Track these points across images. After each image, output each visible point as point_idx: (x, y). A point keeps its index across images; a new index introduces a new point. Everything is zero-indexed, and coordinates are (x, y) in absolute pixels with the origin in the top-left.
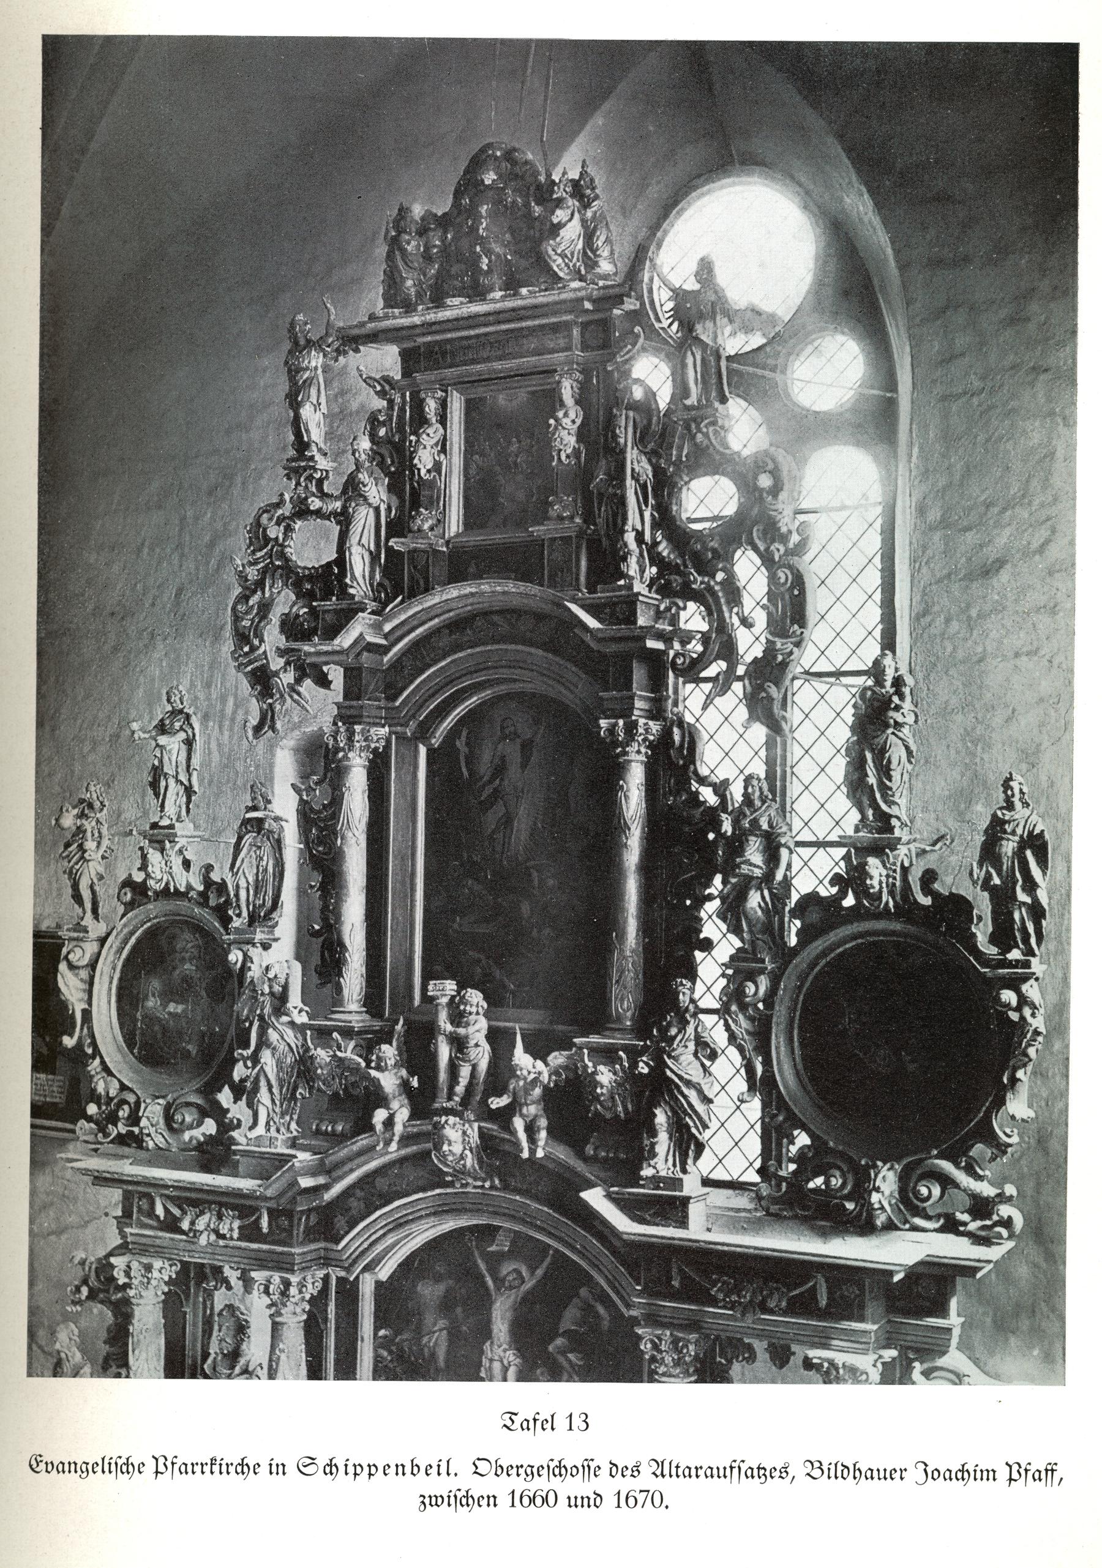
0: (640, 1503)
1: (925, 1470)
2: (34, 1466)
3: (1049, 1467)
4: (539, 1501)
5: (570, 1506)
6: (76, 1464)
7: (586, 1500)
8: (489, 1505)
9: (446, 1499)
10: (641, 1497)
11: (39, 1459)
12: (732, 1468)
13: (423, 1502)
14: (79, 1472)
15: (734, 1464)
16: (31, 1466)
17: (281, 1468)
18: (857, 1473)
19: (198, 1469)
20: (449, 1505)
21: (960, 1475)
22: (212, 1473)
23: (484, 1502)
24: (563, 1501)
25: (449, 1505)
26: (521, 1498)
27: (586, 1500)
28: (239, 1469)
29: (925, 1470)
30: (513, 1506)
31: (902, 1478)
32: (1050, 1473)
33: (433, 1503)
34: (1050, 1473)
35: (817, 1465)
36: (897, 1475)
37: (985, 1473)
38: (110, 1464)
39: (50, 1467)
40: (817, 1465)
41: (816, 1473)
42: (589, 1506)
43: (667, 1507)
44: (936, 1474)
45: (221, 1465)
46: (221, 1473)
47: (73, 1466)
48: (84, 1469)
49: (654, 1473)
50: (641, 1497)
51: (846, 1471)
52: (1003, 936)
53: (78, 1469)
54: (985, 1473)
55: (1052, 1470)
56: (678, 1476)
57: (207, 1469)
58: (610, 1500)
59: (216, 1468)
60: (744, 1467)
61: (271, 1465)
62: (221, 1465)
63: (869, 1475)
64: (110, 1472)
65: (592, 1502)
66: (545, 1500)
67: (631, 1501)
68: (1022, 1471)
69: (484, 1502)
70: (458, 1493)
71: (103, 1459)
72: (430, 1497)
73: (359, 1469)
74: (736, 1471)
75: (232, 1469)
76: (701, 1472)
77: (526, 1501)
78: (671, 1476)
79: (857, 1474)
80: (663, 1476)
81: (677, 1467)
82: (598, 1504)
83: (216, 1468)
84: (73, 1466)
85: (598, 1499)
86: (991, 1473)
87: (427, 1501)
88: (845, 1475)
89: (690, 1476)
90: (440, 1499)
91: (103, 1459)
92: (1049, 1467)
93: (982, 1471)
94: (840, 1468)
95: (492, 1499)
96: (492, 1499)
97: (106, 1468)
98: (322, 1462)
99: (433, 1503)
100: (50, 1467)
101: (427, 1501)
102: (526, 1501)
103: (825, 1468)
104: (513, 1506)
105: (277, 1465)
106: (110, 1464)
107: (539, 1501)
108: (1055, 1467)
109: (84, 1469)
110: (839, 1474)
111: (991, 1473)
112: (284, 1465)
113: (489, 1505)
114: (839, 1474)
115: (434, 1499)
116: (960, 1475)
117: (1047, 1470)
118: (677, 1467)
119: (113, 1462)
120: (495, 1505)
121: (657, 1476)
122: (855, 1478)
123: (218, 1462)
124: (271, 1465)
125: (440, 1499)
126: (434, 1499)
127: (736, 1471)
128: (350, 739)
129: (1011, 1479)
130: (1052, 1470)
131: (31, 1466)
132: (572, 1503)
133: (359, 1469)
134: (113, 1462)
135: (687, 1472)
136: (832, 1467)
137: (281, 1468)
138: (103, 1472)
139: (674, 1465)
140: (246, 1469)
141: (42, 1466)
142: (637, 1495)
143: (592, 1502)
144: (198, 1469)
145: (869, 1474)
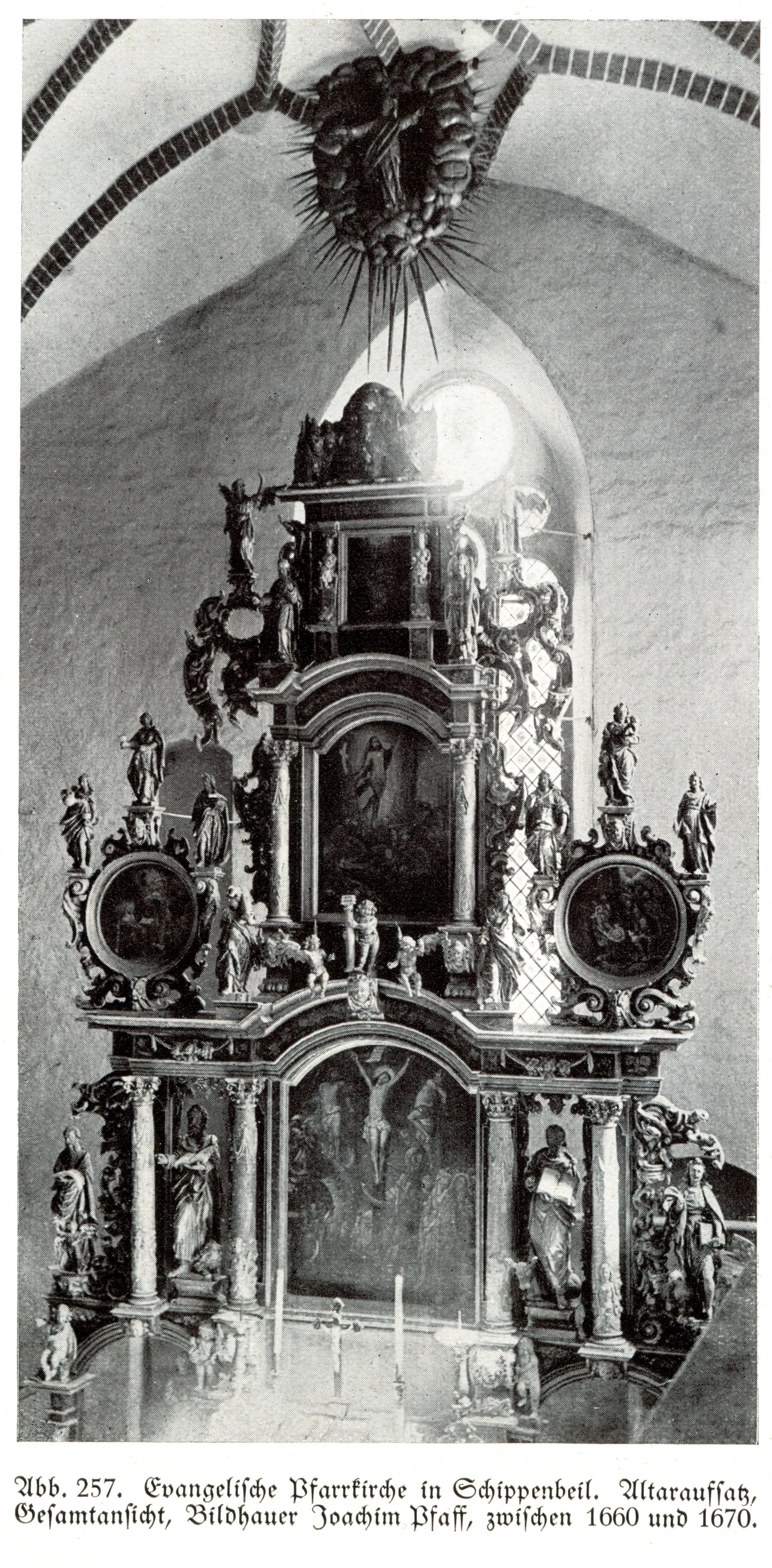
0: (726, 1522)
1: (323, 1515)
2: (151, 1489)
3: (458, 1510)
4: (619, 1519)
5: (652, 1524)
6: (198, 1486)
7: (669, 1519)
8: (562, 1523)
9: (515, 1518)
10: (727, 1517)
11: (156, 1482)
12: (710, 1489)
13: (491, 1521)
14: (202, 1496)
15: (712, 1486)
16: (146, 1489)
17: (435, 1491)
18: (244, 1518)
19: (339, 1492)
20: (518, 1523)
21: (361, 1518)
22: (355, 1496)
23: (557, 1521)
24: (644, 1519)
25: (518, 1523)
26: (602, 1516)
27: (669, 1519)
28: (384, 1492)
29: (323, 1515)
30: (592, 1524)
31: (292, 1523)
32: (459, 1516)
33: (502, 1521)
34: (459, 1516)
35: (199, 1509)
36: (287, 1519)
37: (388, 1517)
38: (237, 1487)
39: (168, 1491)
40: (199, 1509)
41: (199, 1518)
42: (672, 1525)
43: (755, 1525)
44: (335, 1518)
45: (364, 1487)
46: (365, 1496)
47: (195, 1489)
48: (208, 1492)
49: (626, 1495)
50: (727, 1517)
51: (231, 1514)
52: (689, 863)
53: (201, 1492)
54: (388, 1517)
55: (462, 1513)
56: (651, 1498)
57: (349, 1492)
58: (695, 1519)
59: (359, 1491)
60: (724, 1488)
61: (424, 1488)
62: (364, 1487)
63: (256, 1519)
64: (237, 1495)
65: (675, 1521)
66: (626, 1519)
67: (717, 1520)
68: (428, 1514)
69: (557, 1521)
70: (528, 1511)
71: (229, 1482)
72: (499, 1515)
73: (511, 1492)
74: (715, 1493)
75: (376, 1492)
76: (677, 1495)
77: (606, 1519)
78: (643, 1498)
79: (244, 1518)
80: (635, 1497)
81: (651, 1488)
82: (682, 1522)
83: (359, 1491)
84: (195, 1489)
85: (682, 1517)
86: (394, 1517)
87: (495, 1519)
88: (231, 1519)
89: (688, 1498)
90: (509, 1518)
91: (229, 1482)
92: (458, 1510)
93: (384, 1514)
94: (224, 1512)
95: (566, 1517)
96: (566, 1517)
97: (233, 1491)
98: (478, 1484)
99: (502, 1521)
100: (168, 1491)
101: (495, 1519)
102: (606, 1519)
103: (207, 1512)
104: (592, 1524)
105: (431, 1488)
106: (237, 1487)
107: (619, 1519)
108: (464, 1510)
109: (208, 1492)
110: (224, 1518)
111: (394, 1517)
112: (438, 1488)
113: (562, 1523)
114: (224, 1518)
115: (502, 1517)
116: (361, 1518)
117: (455, 1513)
118: (651, 1488)
119: (240, 1485)
120: (569, 1523)
121: (628, 1497)
122: (241, 1523)
123: (361, 1485)
124: (424, 1488)
125: (509, 1518)
126: (502, 1517)
127: (715, 1493)
128: (282, 749)
129: (416, 1523)
130: (462, 1513)
131: (146, 1489)
132: (655, 1521)
133: (511, 1492)
134: (240, 1485)
135: (661, 1494)
136: (216, 1512)
137: (435, 1491)
138: (229, 1495)
139: (647, 1486)
140: (261, 1491)
141: (160, 1490)
142: (723, 1513)
143: (675, 1521)
144: (339, 1492)
145: (256, 1518)
